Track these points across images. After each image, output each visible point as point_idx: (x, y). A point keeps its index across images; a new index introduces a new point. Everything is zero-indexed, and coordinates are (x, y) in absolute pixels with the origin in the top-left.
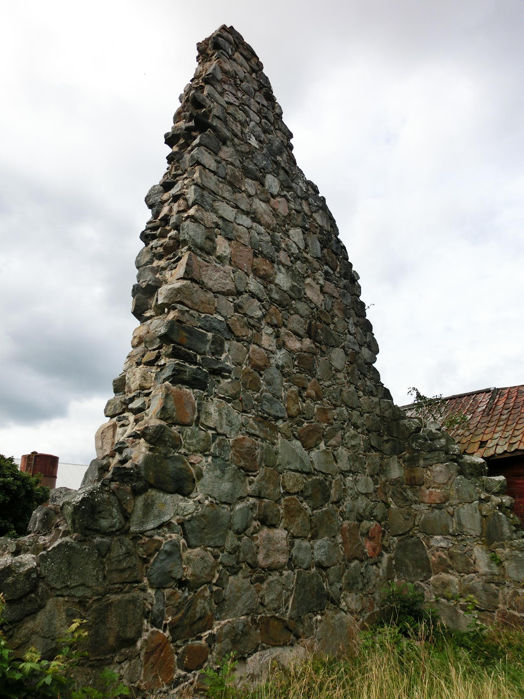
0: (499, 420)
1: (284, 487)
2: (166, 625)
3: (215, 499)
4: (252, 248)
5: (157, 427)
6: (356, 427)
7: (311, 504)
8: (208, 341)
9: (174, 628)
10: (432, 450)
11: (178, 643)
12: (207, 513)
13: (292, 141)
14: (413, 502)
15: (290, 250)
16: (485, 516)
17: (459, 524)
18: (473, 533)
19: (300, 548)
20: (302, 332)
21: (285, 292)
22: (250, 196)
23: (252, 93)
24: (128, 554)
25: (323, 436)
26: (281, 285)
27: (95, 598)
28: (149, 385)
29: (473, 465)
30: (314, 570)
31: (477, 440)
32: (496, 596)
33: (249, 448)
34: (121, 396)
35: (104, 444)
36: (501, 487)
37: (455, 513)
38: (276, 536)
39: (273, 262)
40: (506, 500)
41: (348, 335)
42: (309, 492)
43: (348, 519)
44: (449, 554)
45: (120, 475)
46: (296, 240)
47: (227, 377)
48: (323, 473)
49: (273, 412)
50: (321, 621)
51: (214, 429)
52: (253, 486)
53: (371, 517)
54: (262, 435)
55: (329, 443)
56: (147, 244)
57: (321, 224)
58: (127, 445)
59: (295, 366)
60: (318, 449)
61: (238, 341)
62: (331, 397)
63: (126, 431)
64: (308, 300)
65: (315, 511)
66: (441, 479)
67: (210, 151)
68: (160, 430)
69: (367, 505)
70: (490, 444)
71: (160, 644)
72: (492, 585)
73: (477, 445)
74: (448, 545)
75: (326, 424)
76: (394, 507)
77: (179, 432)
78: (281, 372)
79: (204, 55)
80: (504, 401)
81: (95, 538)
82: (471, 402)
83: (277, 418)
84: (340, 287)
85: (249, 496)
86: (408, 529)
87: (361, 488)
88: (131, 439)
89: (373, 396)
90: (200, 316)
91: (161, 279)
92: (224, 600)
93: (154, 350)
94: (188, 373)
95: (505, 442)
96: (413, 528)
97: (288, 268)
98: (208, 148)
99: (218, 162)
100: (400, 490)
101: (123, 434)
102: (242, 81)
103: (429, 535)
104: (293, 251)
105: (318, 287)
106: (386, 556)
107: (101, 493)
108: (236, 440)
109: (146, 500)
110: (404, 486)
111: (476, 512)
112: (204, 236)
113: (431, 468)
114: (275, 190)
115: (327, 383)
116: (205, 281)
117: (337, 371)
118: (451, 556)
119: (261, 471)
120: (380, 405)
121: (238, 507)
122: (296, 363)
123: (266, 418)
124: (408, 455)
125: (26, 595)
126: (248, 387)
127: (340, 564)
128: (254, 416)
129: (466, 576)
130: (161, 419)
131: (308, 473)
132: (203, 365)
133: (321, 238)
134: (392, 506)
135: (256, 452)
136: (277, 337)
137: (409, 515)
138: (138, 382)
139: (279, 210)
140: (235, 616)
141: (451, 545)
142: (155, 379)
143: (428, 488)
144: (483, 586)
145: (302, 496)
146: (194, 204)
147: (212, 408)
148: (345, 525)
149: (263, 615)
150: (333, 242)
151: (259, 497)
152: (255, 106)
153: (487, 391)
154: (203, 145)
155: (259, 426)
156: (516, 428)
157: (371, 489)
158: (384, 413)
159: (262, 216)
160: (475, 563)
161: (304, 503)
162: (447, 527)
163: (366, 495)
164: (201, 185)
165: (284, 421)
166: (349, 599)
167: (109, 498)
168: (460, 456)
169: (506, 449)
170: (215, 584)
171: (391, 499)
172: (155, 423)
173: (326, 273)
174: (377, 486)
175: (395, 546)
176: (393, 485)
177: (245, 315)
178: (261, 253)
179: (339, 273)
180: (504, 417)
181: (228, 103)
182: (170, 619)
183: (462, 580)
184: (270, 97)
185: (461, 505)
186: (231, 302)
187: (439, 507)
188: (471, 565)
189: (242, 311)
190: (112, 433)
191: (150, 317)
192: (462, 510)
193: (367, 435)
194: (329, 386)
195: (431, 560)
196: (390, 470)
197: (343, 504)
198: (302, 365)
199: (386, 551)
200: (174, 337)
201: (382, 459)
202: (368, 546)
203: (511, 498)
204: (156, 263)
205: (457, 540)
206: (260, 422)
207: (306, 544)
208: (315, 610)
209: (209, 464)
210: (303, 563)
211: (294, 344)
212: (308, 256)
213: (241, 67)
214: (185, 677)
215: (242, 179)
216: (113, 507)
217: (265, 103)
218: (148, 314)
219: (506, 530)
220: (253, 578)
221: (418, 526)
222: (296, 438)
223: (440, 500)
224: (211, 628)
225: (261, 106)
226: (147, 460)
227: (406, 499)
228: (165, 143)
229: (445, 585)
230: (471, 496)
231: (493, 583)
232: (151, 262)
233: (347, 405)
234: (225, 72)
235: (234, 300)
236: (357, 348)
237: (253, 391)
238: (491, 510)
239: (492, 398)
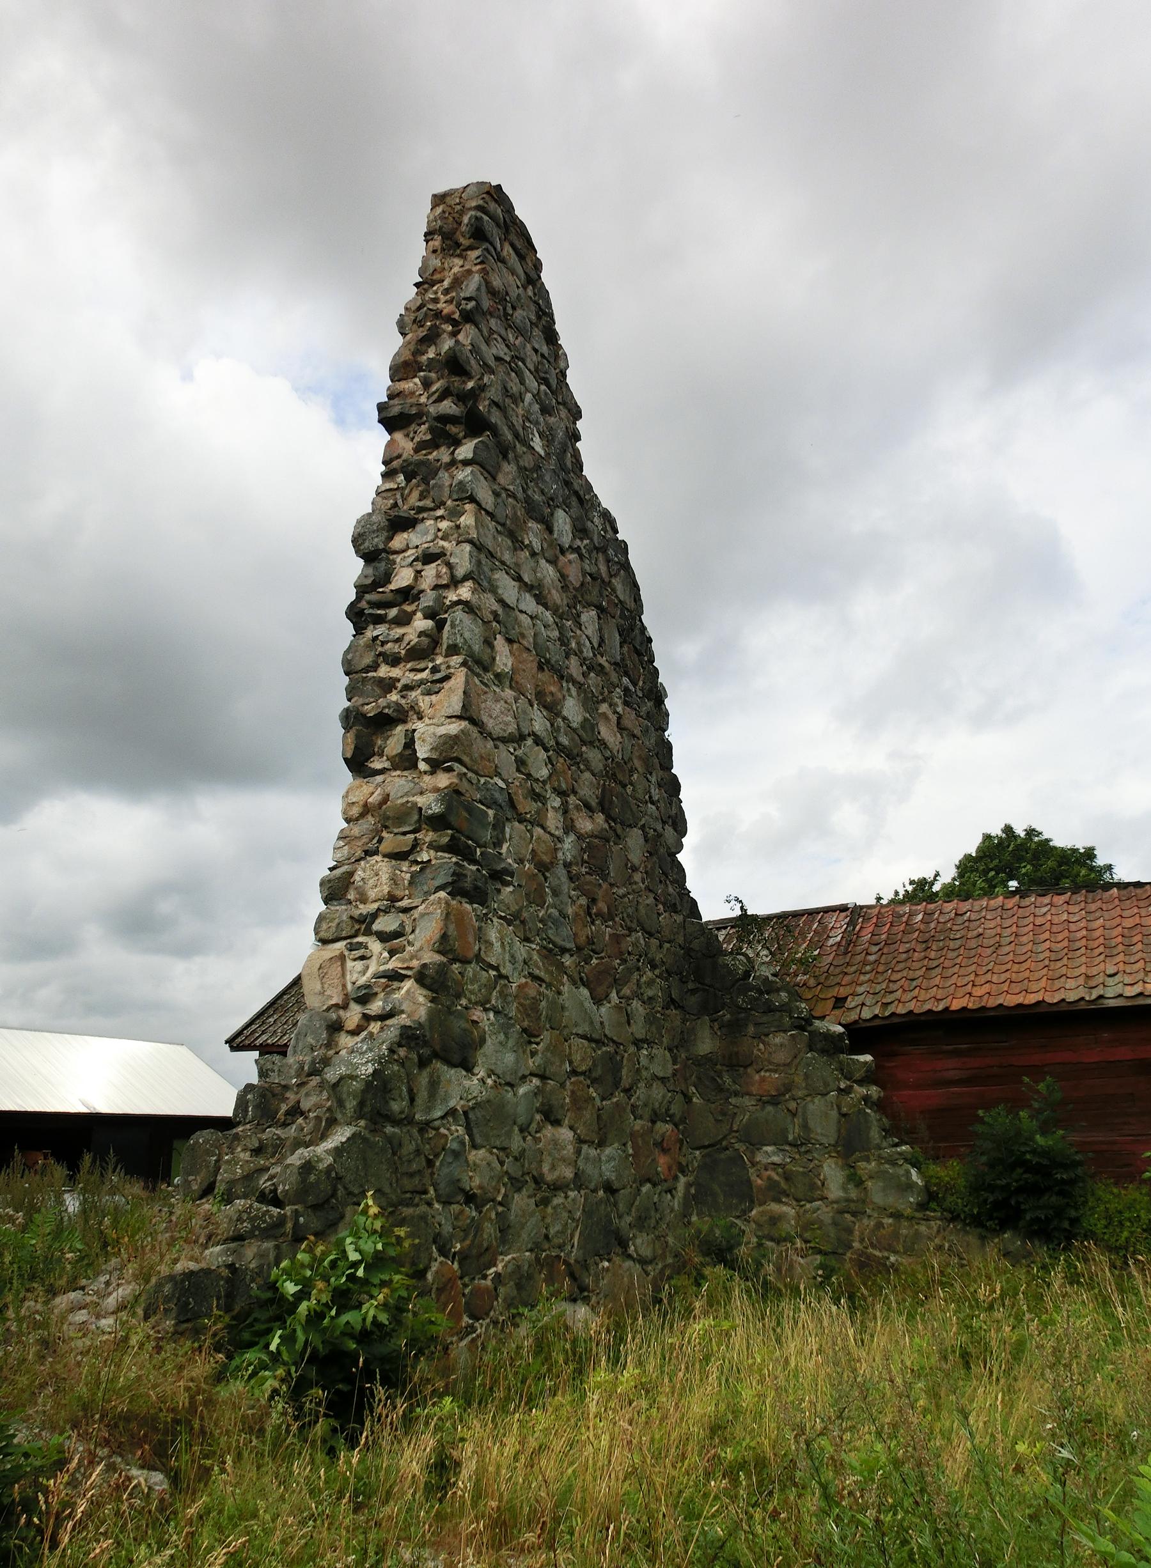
0: (865, 963)
1: (571, 1063)
2: (455, 1253)
3: (499, 1078)
4: (537, 655)
5: (439, 965)
6: (654, 967)
7: (600, 1090)
8: (490, 823)
9: (463, 1258)
10: (770, 1009)
11: (466, 1280)
12: (492, 1098)
13: (580, 425)
14: (731, 1094)
15: (582, 652)
16: (844, 1115)
17: (805, 1126)
18: (825, 1141)
19: (587, 1159)
20: (594, 803)
21: (574, 730)
22: (534, 554)
23: (527, 331)
24: (418, 1152)
25: (615, 980)
26: (570, 718)
27: (391, 1209)
28: (402, 894)
29: (828, 1036)
30: (601, 1193)
31: (830, 995)
32: (850, 1231)
33: (533, 998)
34: (344, 907)
35: (326, 986)
36: (867, 1071)
37: (800, 1110)
38: (563, 1137)
39: (562, 677)
40: (874, 1091)
41: (649, 805)
42: (598, 1073)
43: (641, 1118)
44: (785, 1173)
45: (408, 1037)
46: (589, 632)
47: (508, 884)
48: (614, 1042)
49: (560, 942)
50: (608, 1269)
51: (496, 968)
52: (538, 1059)
53: (668, 1117)
54: (547, 977)
55: (622, 993)
56: (359, 630)
57: (622, 598)
58: (376, 990)
59: (584, 862)
60: (610, 1002)
61: (520, 822)
62: (625, 915)
63: (367, 968)
64: (604, 744)
65: (604, 1103)
66: (781, 1057)
67: (486, 475)
68: (442, 969)
69: (664, 1097)
70: (851, 1003)
71: (450, 1279)
72: (846, 1215)
73: (831, 1003)
74: (783, 1160)
75: (618, 961)
76: (698, 1101)
77: (460, 973)
78: (569, 872)
79: (448, 242)
80: (871, 929)
81: (385, 1127)
82: (815, 926)
83: (564, 951)
84: (641, 717)
85: (532, 1074)
86: (721, 1137)
87: (659, 1071)
88: (383, 980)
89: (676, 912)
90: (479, 781)
91: (405, 706)
92: (509, 1226)
93: (404, 834)
94: (469, 879)
95: (874, 1001)
96: (729, 1134)
97: (579, 686)
98: (484, 468)
99: (496, 494)
100: (712, 1074)
101: (364, 972)
102: (514, 308)
103: (755, 1144)
104: (585, 654)
105: (614, 718)
106: (682, 1180)
107: (390, 1063)
108: (519, 986)
109: (431, 1076)
110: (719, 1067)
111: (832, 1109)
112: (482, 639)
113: (766, 1039)
114: (566, 540)
115: (622, 891)
116: (485, 719)
117: (634, 869)
118: (787, 1177)
119: (546, 1036)
120: (685, 928)
121: (522, 1091)
122: (586, 857)
123: (550, 951)
124: (728, 1016)
125: (327, 1201)
126: (531, 900)
127: (631, 1187)
128: (538, 948)
129: (808, 1206)
130: (439, 952)
131: (597, 1042)
132: (483, 864)
133: (622, 626)
134: (694, 1100)
135: (541, 1007)
136: (565, 812)
137: (724, 1114)
138: (386, 889)
139: (570, 578)
140: (519, 1250)
141: (788, 1160)
142: (410, 883)
143: (758, 1072)
144: (833, 1218)
145: (589, 1078)
146: (466, 578)
147: (493, 935)
148: (637, 1128)
149: (548, 1252)
150: (637, 631)
151: (543, 1077)
152: (532, 359)
153: (843, 908)
154: (477, 464)
155: (543, 964)
156: (892, 978)
157: (670, 1068)
158: (691, 942)
159: (549, 592)
160: (823, 1184)
161: (591, 1090)
162: (784, 1132)
163: (663, 1080)
164: (478, 543)
165: (572, 955)
166: (639, 1241)
167: (399, 1071)
168: (808, 1021)
169: (877, 1012)
170: (500, 1204)
171: (693, 1088)
172: (432, 958)
173: (626, 690)
174: (675, 1067)
175: (696, 1164)
176: (699, 1065)
177: (529, 775)
178: (548, 661)
179: (642, 690)
180: (872, 958)
181: (498, 359)
182: (458, 1246)
183: (802, 1211)
184: (551, 337)
185: (809, 1099)
186: (512, 754)
187: (775, 1101)
188: (818, 1188)
189: (525, 769)
190: (339, 968)
191: (382, 771)
192: (811, 1107)
193: (667, 980)
194: (624, 896)
195: (754, 1184)
196: (695, 1039)
197: (635, 1093)
198: (592, 861)
199: (683, 1172)
200: (453, 819)
201: (684, 1021)
202: (663, 1162)
203: (879, 1089)
204: (384, 671)
205: (799, 1153)
206: (546, 957)
207: (593, 1152)
208: (601, 1252)
209: (492, 1024)
210: (590, 1182)
211: (586, 825)
212: (602, 661)
213: (513, 274)
214: (472, 1326)
215: (525, 522)
216: (403, 1083)
217: (545, 349)
218: (377, 764)
219: (875, 1134)
220: (537, 1198)
221: (737, 1132)
222: (584, 985)
223: (777, 1090)
224: (495, 1265)
225: (540, 359)
226: (432, 1015)
227: (720, 1089)
228: (379, 422)
229: (774, 1220)
230: (826, 1084)
231: (848, 1212)
232: (375, 667)
233: (643, 929)
234: (492, 292)
235: (515, 750)
236: (659, 827)
237: (538, 906)
238: (855, 1106)
239: (852, 923)
